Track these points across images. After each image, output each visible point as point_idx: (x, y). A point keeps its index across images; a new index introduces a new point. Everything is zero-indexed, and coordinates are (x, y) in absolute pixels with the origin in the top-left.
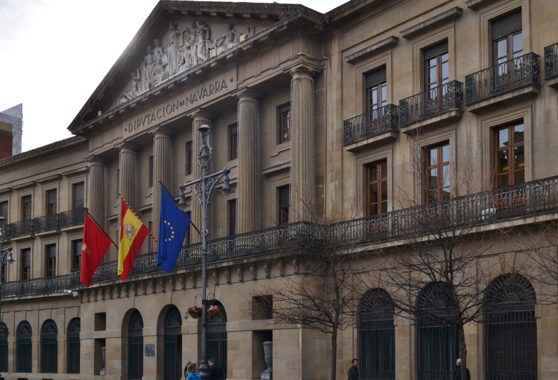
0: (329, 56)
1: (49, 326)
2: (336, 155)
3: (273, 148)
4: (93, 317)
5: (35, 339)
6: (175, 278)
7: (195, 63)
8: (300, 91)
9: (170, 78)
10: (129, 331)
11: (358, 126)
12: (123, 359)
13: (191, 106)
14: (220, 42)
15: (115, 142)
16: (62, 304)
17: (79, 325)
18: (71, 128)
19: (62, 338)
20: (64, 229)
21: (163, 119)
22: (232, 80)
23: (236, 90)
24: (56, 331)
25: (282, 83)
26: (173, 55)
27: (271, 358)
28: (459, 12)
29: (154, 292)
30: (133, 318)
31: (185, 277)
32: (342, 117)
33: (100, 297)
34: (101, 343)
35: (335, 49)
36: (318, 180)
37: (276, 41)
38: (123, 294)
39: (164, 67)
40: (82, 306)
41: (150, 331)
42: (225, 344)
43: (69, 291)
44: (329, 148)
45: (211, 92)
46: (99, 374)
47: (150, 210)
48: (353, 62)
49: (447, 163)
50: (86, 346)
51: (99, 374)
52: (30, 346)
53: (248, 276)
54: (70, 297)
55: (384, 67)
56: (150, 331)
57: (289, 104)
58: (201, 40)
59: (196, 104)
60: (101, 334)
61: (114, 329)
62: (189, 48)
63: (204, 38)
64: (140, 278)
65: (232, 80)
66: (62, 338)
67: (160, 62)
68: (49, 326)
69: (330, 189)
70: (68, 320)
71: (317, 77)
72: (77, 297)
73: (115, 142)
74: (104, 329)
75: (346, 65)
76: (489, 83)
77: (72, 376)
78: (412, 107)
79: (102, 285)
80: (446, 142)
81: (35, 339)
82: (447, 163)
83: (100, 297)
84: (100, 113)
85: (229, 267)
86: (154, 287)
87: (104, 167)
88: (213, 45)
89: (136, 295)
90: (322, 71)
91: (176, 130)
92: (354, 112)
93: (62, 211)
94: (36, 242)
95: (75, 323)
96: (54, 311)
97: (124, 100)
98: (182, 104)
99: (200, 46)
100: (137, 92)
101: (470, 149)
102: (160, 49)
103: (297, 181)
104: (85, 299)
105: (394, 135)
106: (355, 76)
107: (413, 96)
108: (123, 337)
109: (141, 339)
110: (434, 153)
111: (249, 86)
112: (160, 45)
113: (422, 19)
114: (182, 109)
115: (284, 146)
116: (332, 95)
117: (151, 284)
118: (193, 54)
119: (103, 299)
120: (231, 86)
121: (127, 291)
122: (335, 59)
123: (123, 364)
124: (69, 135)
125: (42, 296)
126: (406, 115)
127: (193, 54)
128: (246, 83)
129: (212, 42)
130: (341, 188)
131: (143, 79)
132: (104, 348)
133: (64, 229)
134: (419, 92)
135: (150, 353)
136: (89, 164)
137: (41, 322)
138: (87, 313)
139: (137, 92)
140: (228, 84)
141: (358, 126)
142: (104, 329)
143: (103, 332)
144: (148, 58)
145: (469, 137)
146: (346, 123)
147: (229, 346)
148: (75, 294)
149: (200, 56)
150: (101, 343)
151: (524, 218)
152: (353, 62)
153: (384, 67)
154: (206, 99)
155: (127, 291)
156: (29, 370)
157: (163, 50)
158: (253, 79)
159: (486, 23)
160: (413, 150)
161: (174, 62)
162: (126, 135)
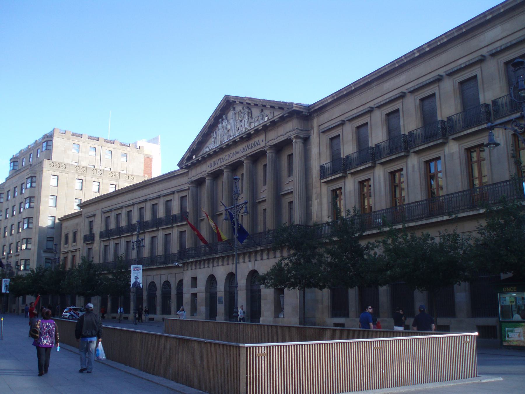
0: (312, 128)
1: (167, 284)
2: (318, 185)
3: (286, 180)
4: (190, 279)
5: (159, 293)
6: (256, 252)
7: (244, 130)
8: (297, 148)
9: (231, 138)
10: (229, 287)
11: (419, 135)
12: (206, 306)
13: (242, 154)
14: (256, 119)
15: (203, 173)
16: (174, 271)
17: (183, 284)
18: (179, 165)
19: (174, 292)
20: (175, 225)
21: (228, 161)
22: (262, 141)
23: (265, 147)
24: (170, 288)
25: (288, 143)
26: (233, 125)
27: (284, 305)
28: (440, 77)
29: (223, 265)
30: (212, 280)
31: (262, 251)
32: (320, 163)
33: (194, 267)
34: (194, 295)
35: (315, 123)
36: (308, 199)
37: (283, 120)
38: (206, 266)
39: (228, 131)
40: (184, 272)
41: (221, 288)
42: (260, 296)
43: (177, 264)
44: (314, 180)
45: (252, 147)
46: (278, 317)
47: (222, 214)
48: (324, 132)
49: (440, 172)
50: (187, 297)
51: (278, 317)
52: (170, 297)
53: (271, 255)
54: (177, 267)
55: (434, 95)
56: (221, 288)
57: (292, 154)
58: (247, 117)
59: (245, 153)
60: (194, 290)
61: (201, 287)
62: (241, 121)
63: (248, 116)
64: (215, 256)
65: (262, 141)
66: (174, 292)
67: (226, 128)
68: (167, 284)
69: (315, 203)
70: (177, 281)
71: (306, 140)
72: (181, 267)
73: (203, 173)
74: (196, 287)
75: (321, 134)
76: (388, 148)
77: (345, 325)
78: (456, 121)
79: (195, 260)
80: (439, 158)
81: (159, 293)
82: (440, 172)
83: (194, 267)
84: (194, 157)
85: (261, 250)
86: (223, 261)
87: (197, 188)
88: (253, 121)
89: (213, 266)
90: (309, 137)
91: (235, 167)
92: (326, 160)
93: (174, 213)
94: (159, 232)
95: (181, 283)
96: (169, 275)
97: (207, 150)
98: (238, 153)
99: (246, 121)
100: (212, 145)
101: (380, 183)
102: (226, 121)
103: (297, 200)
104: (186, 268)
105: (344, 175)
106: (326, 138)
107: (456, 114)
108: (206, 292)
109: (216, 293)
110: (432, 164)
111: (272, 144)
112: (226, 119)
113: (355, 111)
114: (238, 156)
115: (291, 179)
116: (314, 150)
117: (248, 255)
118: (243, 125)
119: (196, 269)
120: (262, 144)
121: (208, 264)
122: (316, 130)
123: (206, 309)
124: (178, 168)
125: (163, 266)
126: (496, 111)
127: (243, 125)
128: (270, 142)
129: (252, 119)
130: (321, 204)
131: (217, 137)
132: (282, 295)
133: (175, 225)
134: (420, 127)
135: (221, 302)
136: (189, 186)
137: (162, 282)
138: (187, 276)
139: (212, 145)
140: (261, 142)
141: (419, 135)
142: (196, 287)
143: (196, 289)
144: (220, 126)
145: (379, 176)
146: (321, 167)
147: (262, 297)
148: (181, 265)
149: (246, 126)
150: (194, 295)
151: (416, 222)
152: (324, 132)
153: (434, 95)
154: (250, 151)
155: (208, 264)
156: (155, 313)
157: (228, 121)
158: (273, 141)
159: (502, 65)
160: (419, 162)
161: (233, 129)
162: (209, 169)
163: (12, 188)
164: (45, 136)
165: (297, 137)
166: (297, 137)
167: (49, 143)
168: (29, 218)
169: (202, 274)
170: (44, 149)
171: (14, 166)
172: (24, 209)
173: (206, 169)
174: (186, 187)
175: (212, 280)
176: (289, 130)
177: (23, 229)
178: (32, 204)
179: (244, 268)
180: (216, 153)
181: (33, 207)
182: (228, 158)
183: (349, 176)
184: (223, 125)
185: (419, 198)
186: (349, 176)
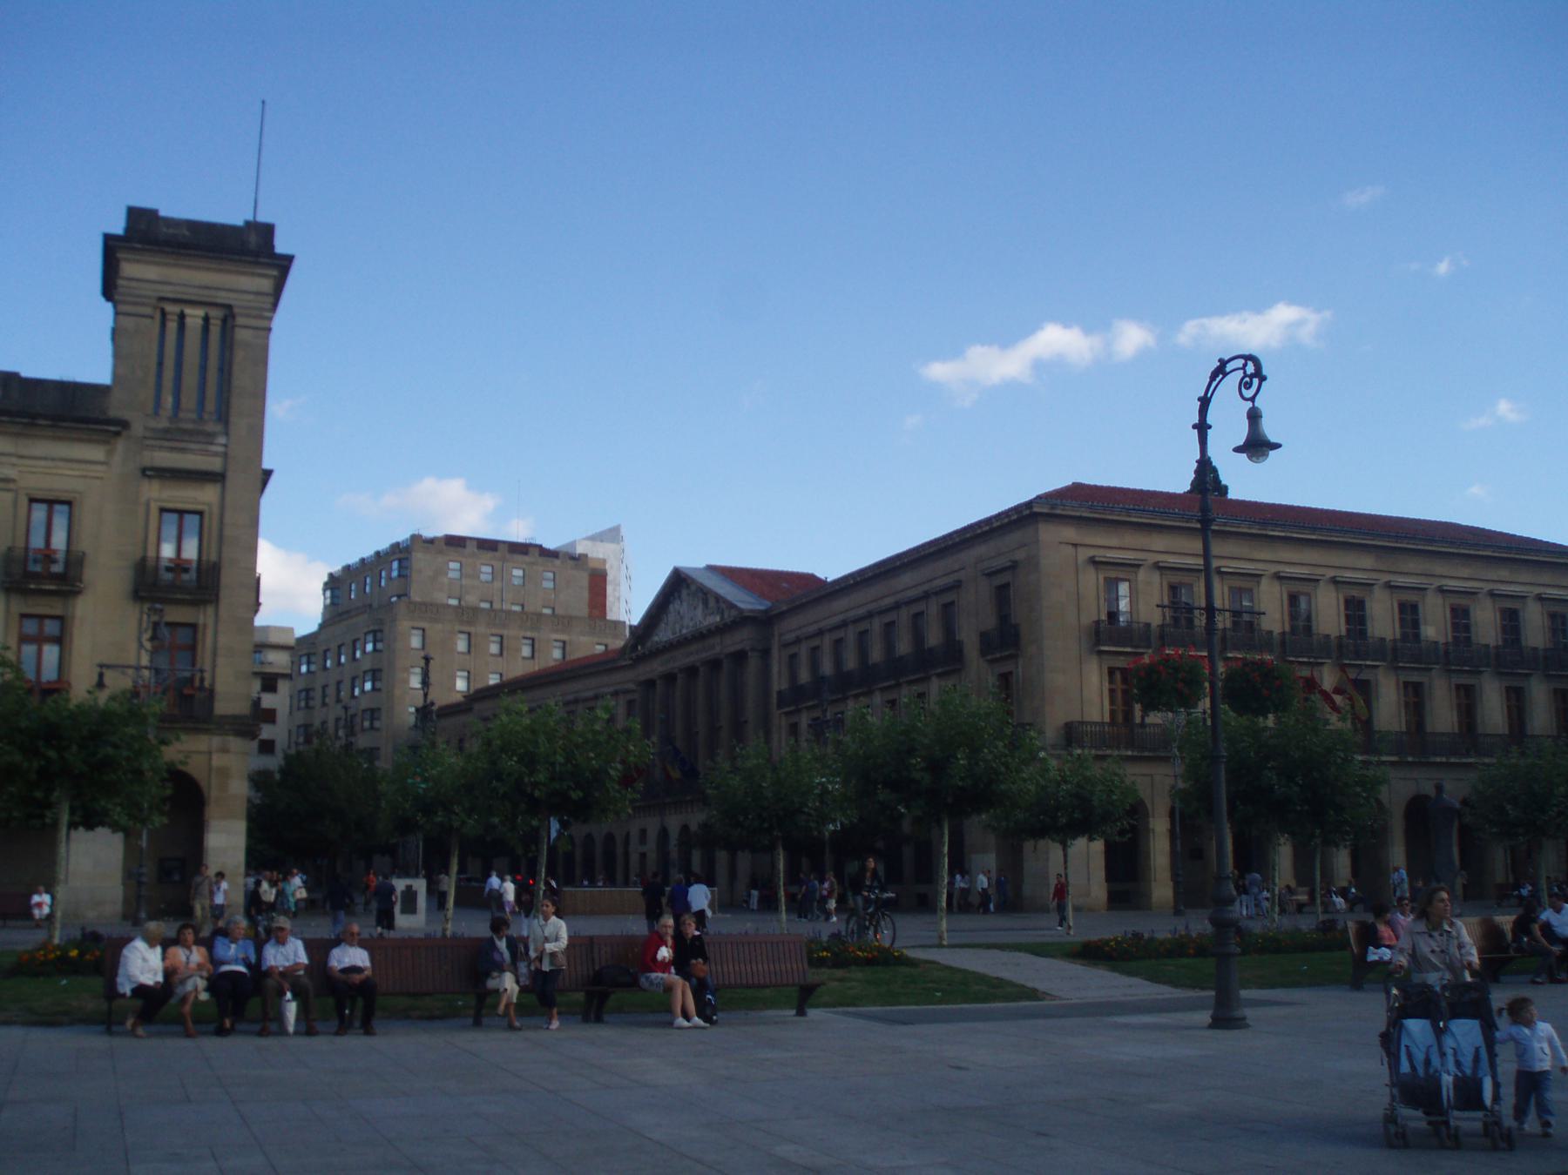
1: (610, 838)
8: (753, 663)
19: (619, 850)
30: (664, 834)
34: (643, 855)
61: (651, 847)
71: (765, 653)
100: (663, 635)
120: (718, 649)
150: (643, 855)
163: (334, 646)
164: (396, 547)
165: (753, 649)
166: (753, 649)
167: (405, 563)
168: (373, 711)
169: (652, 825)
170: (395, 574)
171: (332, 597)
172: (364, 651)
173: (656, 668)
174: (632, 686)
175: (664, 834)
176: (741, 639)
177: (364, 651)
178: (378, 685)
179: (674, 823)
180: (671, 646)
181: (378, 730)
182: (681, 660)
183: (934, 679)
184: (675, 607)
185: (1096, 717)
186: (934, 679)
